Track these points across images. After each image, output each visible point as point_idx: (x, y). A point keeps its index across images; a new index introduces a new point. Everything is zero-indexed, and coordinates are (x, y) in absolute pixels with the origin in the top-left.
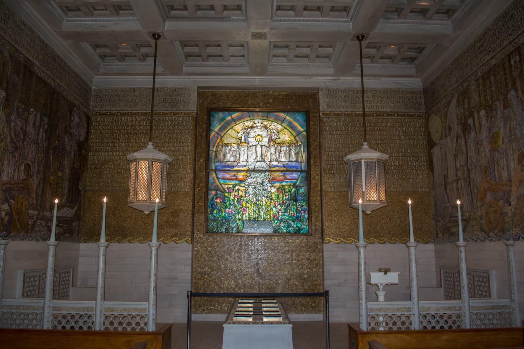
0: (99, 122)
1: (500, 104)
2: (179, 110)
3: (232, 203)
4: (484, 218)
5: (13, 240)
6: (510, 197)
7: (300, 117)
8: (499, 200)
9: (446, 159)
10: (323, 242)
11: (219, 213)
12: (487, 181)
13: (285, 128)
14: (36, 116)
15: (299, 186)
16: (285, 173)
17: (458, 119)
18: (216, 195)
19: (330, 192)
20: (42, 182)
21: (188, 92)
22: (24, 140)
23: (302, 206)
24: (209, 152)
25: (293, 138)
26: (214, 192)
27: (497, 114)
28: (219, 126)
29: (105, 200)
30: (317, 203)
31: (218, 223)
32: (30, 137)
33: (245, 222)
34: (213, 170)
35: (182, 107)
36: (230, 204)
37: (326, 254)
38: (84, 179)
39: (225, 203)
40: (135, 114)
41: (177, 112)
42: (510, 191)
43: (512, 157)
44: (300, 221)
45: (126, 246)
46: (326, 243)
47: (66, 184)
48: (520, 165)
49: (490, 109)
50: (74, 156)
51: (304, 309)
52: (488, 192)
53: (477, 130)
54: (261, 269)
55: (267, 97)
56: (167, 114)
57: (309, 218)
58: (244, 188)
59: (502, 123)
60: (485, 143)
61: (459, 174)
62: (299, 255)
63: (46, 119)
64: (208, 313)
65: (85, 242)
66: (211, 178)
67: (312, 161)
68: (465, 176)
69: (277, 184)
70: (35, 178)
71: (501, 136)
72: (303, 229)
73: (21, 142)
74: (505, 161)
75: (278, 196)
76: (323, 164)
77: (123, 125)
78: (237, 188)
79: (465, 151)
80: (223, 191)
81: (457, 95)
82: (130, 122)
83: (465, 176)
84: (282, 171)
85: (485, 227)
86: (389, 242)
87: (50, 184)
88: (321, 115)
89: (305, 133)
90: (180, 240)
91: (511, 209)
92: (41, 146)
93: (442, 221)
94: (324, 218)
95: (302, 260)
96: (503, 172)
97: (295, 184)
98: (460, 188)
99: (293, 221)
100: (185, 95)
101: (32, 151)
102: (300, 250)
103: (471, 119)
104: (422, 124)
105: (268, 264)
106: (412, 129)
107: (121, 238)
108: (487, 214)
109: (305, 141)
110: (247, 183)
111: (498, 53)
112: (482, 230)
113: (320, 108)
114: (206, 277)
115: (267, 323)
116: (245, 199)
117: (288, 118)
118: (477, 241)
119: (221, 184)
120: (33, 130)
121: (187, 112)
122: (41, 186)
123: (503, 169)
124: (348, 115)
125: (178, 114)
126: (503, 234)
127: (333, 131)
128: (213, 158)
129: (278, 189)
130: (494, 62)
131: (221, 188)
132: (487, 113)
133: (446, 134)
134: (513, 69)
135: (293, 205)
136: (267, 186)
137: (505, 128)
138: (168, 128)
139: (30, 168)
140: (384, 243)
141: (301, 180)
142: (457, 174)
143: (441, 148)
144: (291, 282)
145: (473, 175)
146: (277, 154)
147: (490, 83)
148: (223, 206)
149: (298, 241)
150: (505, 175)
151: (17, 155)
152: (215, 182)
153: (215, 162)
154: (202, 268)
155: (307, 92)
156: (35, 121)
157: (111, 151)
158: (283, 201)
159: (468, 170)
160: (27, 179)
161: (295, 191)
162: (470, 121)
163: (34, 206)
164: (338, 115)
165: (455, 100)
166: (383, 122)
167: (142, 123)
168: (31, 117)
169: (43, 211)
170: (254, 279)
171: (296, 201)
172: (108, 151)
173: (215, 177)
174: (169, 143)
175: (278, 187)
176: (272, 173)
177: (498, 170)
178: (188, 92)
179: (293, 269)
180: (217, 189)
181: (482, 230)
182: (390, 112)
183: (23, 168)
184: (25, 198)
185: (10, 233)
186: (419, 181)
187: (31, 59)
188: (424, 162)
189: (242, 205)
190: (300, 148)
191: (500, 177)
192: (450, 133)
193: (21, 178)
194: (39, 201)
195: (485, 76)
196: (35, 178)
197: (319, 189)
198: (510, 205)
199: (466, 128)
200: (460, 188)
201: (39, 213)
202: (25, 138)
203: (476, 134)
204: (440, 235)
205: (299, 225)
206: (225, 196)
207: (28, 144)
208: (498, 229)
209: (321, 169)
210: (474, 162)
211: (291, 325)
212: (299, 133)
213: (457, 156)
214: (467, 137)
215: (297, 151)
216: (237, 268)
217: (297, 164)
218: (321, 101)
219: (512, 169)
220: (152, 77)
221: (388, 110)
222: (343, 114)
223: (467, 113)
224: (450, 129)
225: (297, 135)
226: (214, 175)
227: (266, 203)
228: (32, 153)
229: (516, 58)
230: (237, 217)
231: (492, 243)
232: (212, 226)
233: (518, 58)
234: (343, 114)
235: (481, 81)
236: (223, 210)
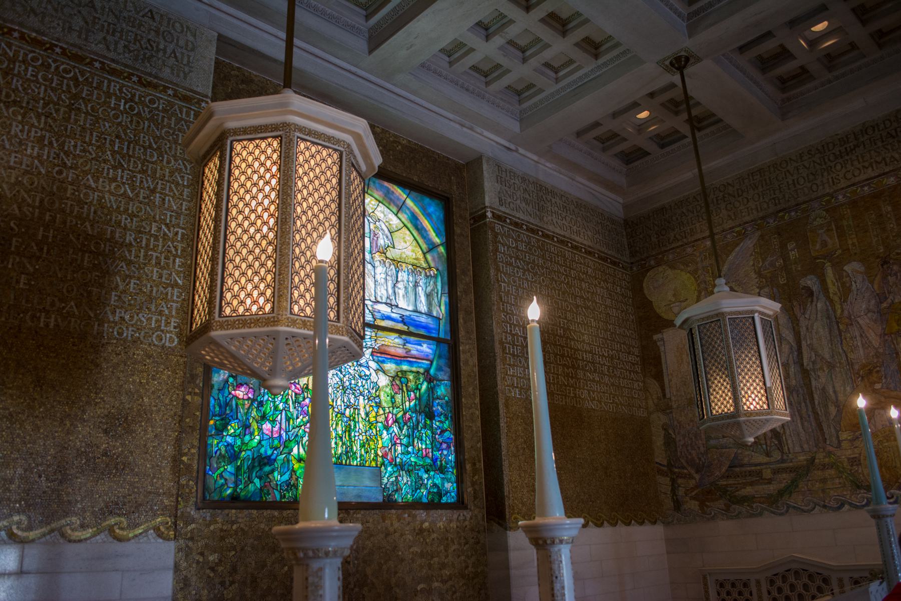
3: (281, 406)
7: (435, 208)
11: (241, 436)
13: (405, 225)
16: (408, 338)
21: (191, 38)
25: (420, 255)
31: (238, 469)
35: (168, 70)
36: (276, 408)
39: (261, 404)
41: (149, 79)
56: (113, 72)
75: (393, 397)
89: (442, 249)
99: (427, 471)
109: (443, 267)
113: (487, 199)
117: (410, 203)
118: (616, 523)
125: (149, 85)
127: (511, 257)
135: (425, 427)
136: (368, 367)
146: (390, 284)
155: (448, 159)
158: (405, 414)
161: (428, 389)
175: (393, 374)
176: (380, 333)
190: (435, 283)
205: (438, 481)
212: (432, 247)
215: (429, 289)
225: (430, 250)
227: (367, 414)
232: (221, 476)
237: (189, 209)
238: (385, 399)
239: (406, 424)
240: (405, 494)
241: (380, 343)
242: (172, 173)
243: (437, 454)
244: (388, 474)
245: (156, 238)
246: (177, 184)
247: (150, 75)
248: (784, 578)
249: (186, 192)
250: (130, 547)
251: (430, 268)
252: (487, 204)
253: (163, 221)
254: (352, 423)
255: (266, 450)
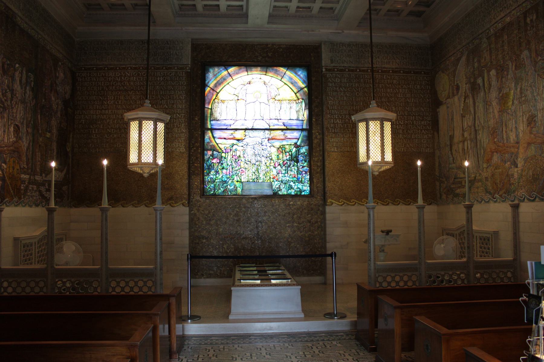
0: (85, 77)
1: (512, 65)
2: (171, 65)
4: (489, 180)
5: (7, 206)
6: (517, 159)
8: (505, 162)
9: (452, 119)
10: (325, 204)
11: (216, 175)
12: (495, 142)
14: (21, 73)
15: (300, 146)
17: (466, 78)
18: (212, 155)
19: (332, 152)
20: (31, 144)
21: (181, 45)
22: (12, 100)
23: (303, 167)
24: (204, 110)
26: (210, 153)
27: (508, 75)
28: (215, 82)
29: (105, 162)
30: (319, 164)
32: (17, 95)
33: (244, 184)
34: (209, 129)
35: (174, 60)
37: (328, 216)
38: (71, 140)
39: (222, 164)
40: (124, 68)
42: (517, 153)
43: (521, 119)
44: (301, 182)
45: (130, 210)
46: (329, 205)
47: (54, 146)
48: (529, 128)
49: (501, 70)
50: (61, 115)
51: (305, 272)
52: (495, 153)
53: (487, 91)
54: (261, 232)
55: (265, 50)
56: (158, 69)
57: (311, 180)
58: (243, 148)
59: (513, 85)
60: (494, 104)
61: (466, 134)
62: (300, 218)
63: (32, 76)
64: (207, 278)
65: (75, 207)
66: (206, 137)
67: (314, 120)
68: (472, 137)
69: (277, 144)
70: (24, 140)
71: (511, 97)
72: (304, 191)
73: (9, 102)
74: (514, 123)
76: (326, 123)
77: (111, 81)
78: (235, 147)
79: (473, 112)
80: (220, 151)
81: (467, 52)
82: (118, 77)
83: (472, 137)
84: (282, 130)
85: (491, 188)
86: (392, 203)
87: (40, 146)
88: (324, 70)
89: (306, 89)
90: (176, 203)
91: (518, 171)
92: (29, 105)
93: (446, 182)
94: (327, 179)
95: (303, 222)
96: (511, 134)
97: (296, 144)
98: (466, 148)
100: (178, 48)
101: (20, 110)
102: (301, 212)
103: (480, 78)
104: (428, 81)
105: (269, 227)
106: (418, 87)
107: (113, 202)
108: (493, 175)
110: (245, 143)
111: (513, 10)
112: (487, 191)
113: (323, 62)
114: (204, 241)
115: (275, 285)
116: (243, 159)
117: (288, 73)
118: (481, 202)
119: (217, 144)
120: (19, 87)
121: (180, 66)
122: (31, 149)
123: (512, 130)
124: (352, 71)
125: (170, 68)
126: (508, 195)
127: (336, 87)
128: (209, 116)
129: (278, 148)
130: (508, 19)
131: (218, 148)
132: (497, 73)
133: (453, 93)
134: (529, 28)
137: (516, 89)
138: (160, 83)
139: (19, 129)
140: (388, 204)
141: (302, 139)
142: (463, 135)
143: (448, 107)
144: (292, 245)
145: (480, 136)
147: (503, 42)
148: (220, 167)
149: (299, 203)
150: (512, 137)
151: (6, 115)
152: (211, 141)
153: (211, 120)
154: (200, 232)
156: (21, 78)
157: (99, 109)
158: (284, 162)
159: (476, 131)
160: (17, 142)
162: (480, 81)
163: (25, 170)
164: (341, 70)
165: (464, 59)
166: (388, 79)
167: (132, 78)
168: (17, 74)
169: (34, 175)
170: (254, 243)
171: (297, 162)
172: (96, 109)
173: (211, 137)
174: (161, 100)
176: (272, 132)
177: (506, 132)
178: (181, 45)
179: (295, 231)
180: (213, 149)
181: (487, 192)
182: (396, 68)
183: (12, 129)
184: (16, 162)
185: (4, 199)
186: (424, 141)
187: (13, 8)
188: (429, 121)
189: (240, 165)
190: (301, 106)
191: (508, 138)
192: (458, 93)
193: (11, 140)
194: (30, 165)
195: (498, 34)
196: (24, 140)
197: (321, 148)
198: (517, 167)
199: (474, 88)
200: (466, 148)
201: (30, 177)
202: (12, 97)
203: (485, 94)
204: (444, 196)
206: (222, 157)
207: (16, 103)
208: (504, 191)
209: (323, 128)
210: (482, 123)
211: (300, 287)
213: (464, 117)
214: (475, 98)
215: (298, 109)
216: (237, 232)
217: (298, 122)
218: (324, 56)
219: (520, 131)
220: (147, 28)
221: (394, 67)
222: (347, 70)
223: (476, 72)
224: (458, 88)
225: (298, 92)
226: (210, 134)
228: (20, 113)
229: (533, 16)
230: (236, 179)
231: (496, 204)
232: (209, 188)
233: (535, 17)
234: (347, 70)
235: (493, 39)
236: (220, 171)
237: (185, 106)
238: (274, 158)
239: (284, 165)
240: (284, 192)
241: (272, 135)
242: (179, 96)
243: (300, 176)
244: (276, 185)
245: (176, 119)
246: (181, 99)
247: (169, 65)
248: (484, 239)
249: (184, 101)
250: (176, 208)
251: (298, 99)
252: (323, 65)
253: (177, 113)
254: (259, 167)
255: (225, 179)
